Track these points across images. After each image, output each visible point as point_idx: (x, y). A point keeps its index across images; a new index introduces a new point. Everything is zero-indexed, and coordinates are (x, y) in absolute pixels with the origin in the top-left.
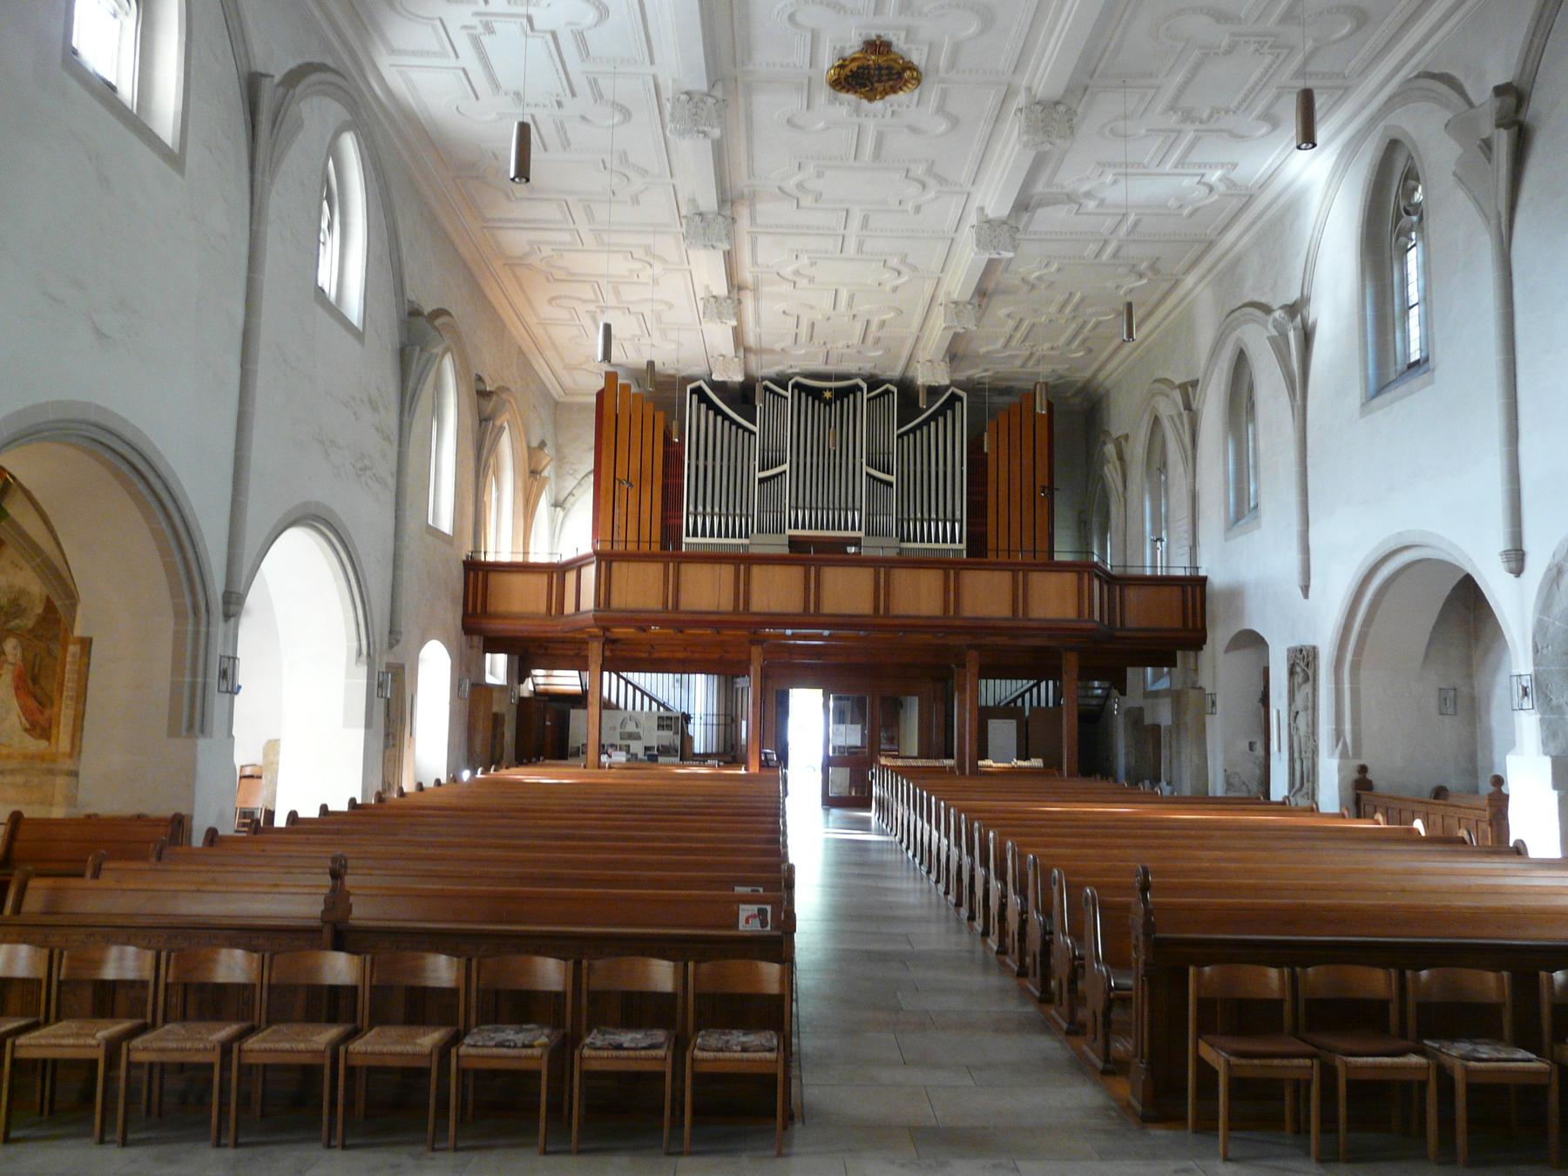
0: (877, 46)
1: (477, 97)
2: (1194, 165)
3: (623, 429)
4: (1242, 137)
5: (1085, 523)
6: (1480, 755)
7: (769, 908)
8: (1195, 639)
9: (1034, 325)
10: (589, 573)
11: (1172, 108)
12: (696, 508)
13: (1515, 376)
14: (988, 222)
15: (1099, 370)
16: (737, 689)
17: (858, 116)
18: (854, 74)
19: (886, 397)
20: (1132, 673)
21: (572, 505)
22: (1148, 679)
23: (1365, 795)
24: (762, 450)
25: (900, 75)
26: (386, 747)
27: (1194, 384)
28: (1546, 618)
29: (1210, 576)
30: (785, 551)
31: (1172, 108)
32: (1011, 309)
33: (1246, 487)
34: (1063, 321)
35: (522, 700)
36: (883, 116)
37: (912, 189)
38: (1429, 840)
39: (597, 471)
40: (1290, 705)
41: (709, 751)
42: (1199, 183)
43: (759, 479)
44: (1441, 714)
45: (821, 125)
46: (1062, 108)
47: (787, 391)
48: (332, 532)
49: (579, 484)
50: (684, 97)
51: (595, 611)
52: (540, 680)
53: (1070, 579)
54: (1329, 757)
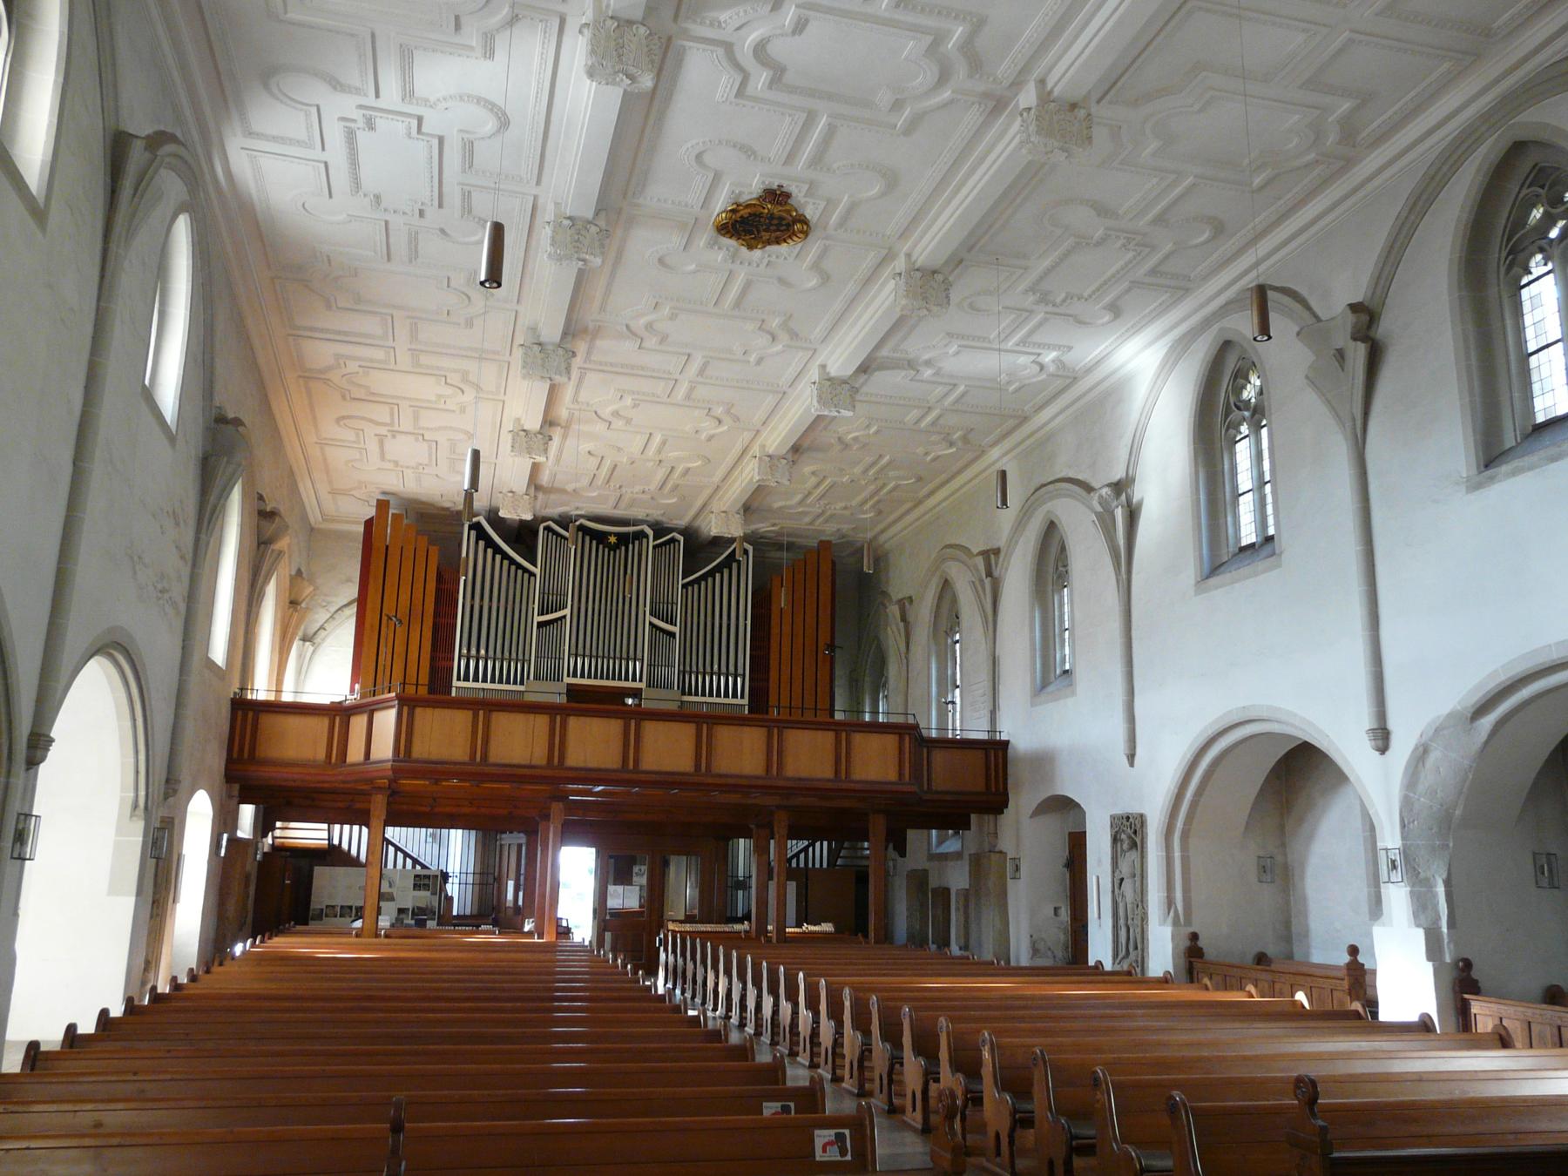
0: (777, 196)
1: (331, 196)
2: (1034, 344)
3: (407, 564)
4: (1085, 323)
5: (857, 681)
6: (1294, 921)
7: (847, 1132)
8: (994, 800)
9: (835, 483)
12: (469, 650)
13: (1373, 565)
14: (829, 380)
15: (882, 532)
16: (501, 845)
17: (733, 262)
18: (743, 220)
19: (672, 545)
20: (912, 835)
21: (323, 640)
22: (927, 843)
23: (1197, 965)
24: (542, 593)
25: (789, 226)
27: (997, 552)
28: (1412, 795)
29: (1012, 741)
30: (564, 699)
31: (1032, 289)
34: (863, 483)
36: (758, 266)
37: (762, 340)
39: (362, 601)
40: (1113, 872)
42: (1033, 362)
43: (538, 623)
44: (1261, 882)
45: (693, 267)
46: (939, 277)
48: (128, 662)
50: (567, 222)
51: (394, 761)
53: (891, 741)
54: (1160, 925)
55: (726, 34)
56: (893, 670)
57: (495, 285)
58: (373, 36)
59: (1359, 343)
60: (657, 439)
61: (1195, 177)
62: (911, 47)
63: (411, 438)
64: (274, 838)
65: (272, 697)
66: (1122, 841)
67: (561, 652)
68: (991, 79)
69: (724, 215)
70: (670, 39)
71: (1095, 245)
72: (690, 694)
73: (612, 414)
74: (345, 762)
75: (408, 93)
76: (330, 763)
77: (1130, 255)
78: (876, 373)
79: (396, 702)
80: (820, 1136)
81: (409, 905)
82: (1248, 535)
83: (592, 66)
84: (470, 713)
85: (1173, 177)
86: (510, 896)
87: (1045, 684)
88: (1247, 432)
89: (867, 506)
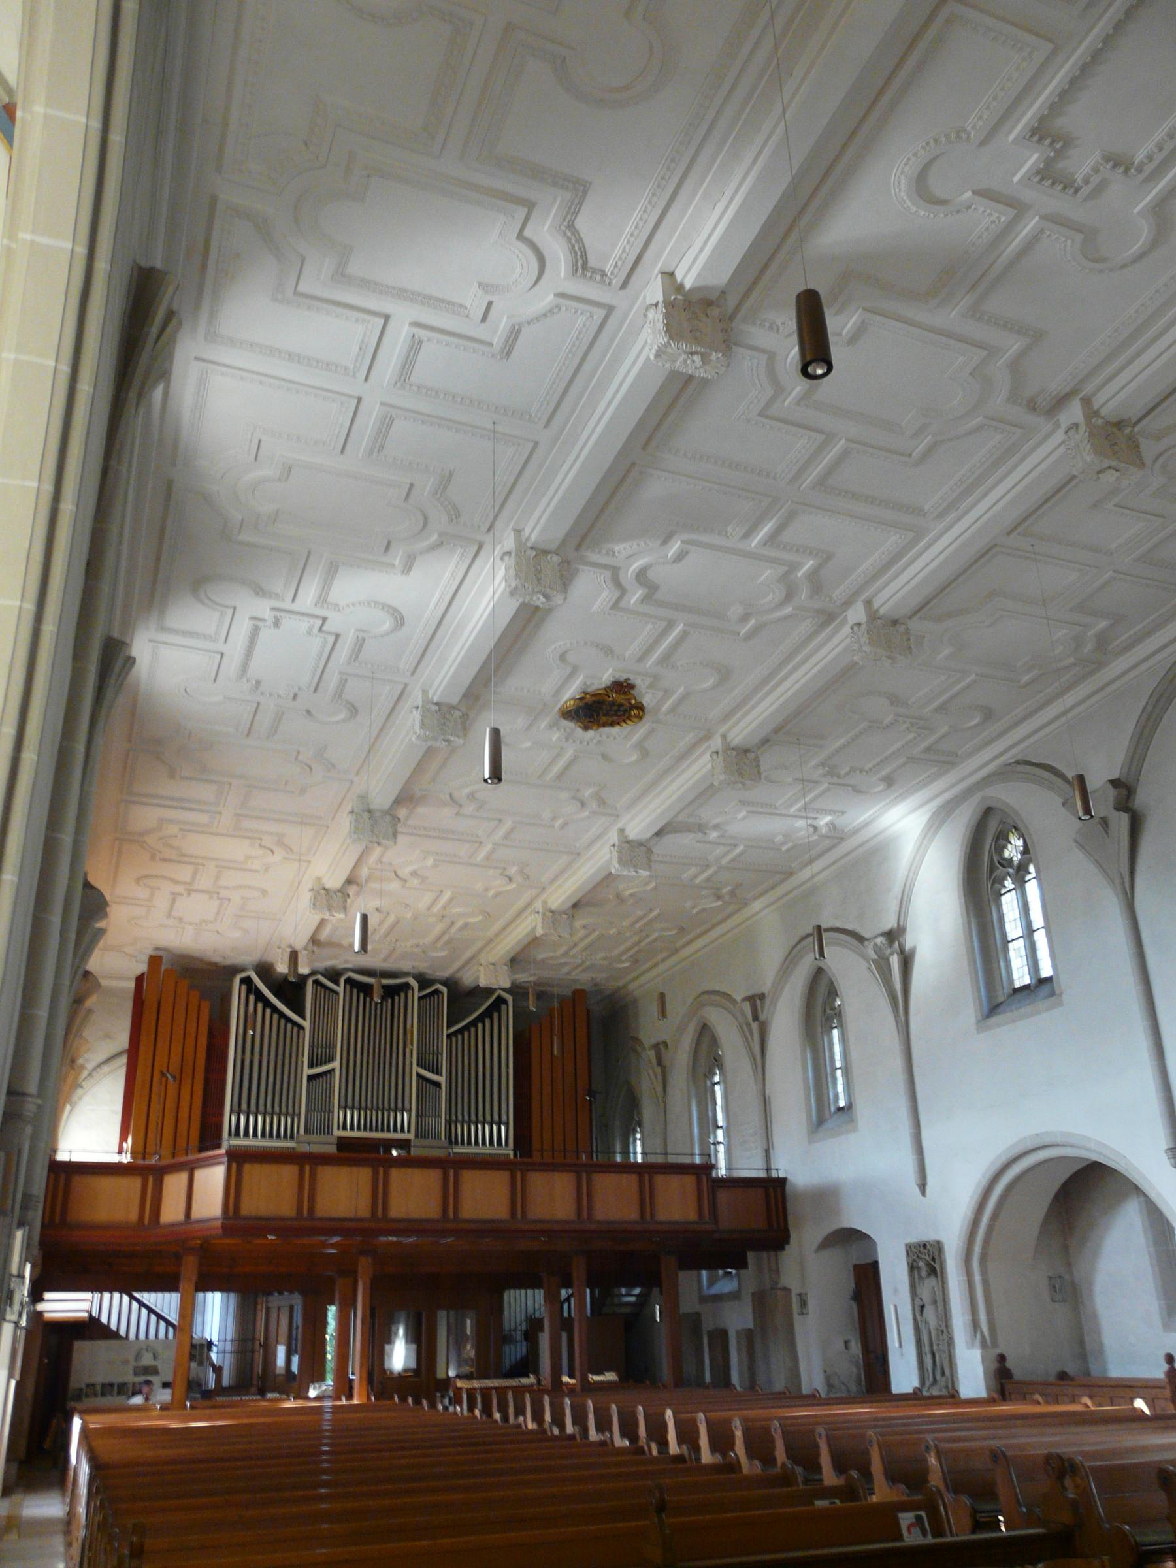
0: (623, 687)
1: (215, 680)
2: (814, 809)
3: (165, 1018)
7: (923, 1514)
11: (823, 764)
14: (628, 842)
21: (80, 1098)
23: (1009, 1387)
24: (312, 1047)
27: (762, 997)
29: (789, 1177)
33: (825, 1091)
38: (1155, 1418)
40: (913, 1300)
45: (528, 744)
53: (689, 1180)
54: (968, 1349)
57: (496, 781)
59: (1122, 813)
60: (447, 895)
61: (977, 675)
62: (768, 573)
63: (206, 896)
66: (919, 1268)
69: (572, 702)
73: (411, 874)
75: (322, 600)
77: (911, 736)
79: (226, 1159)
82: (1021, 977)
83: (516, 588)
86: (281, 1360)
87: (821, 1121)
88: (1012, 886)
89: (624, 958)
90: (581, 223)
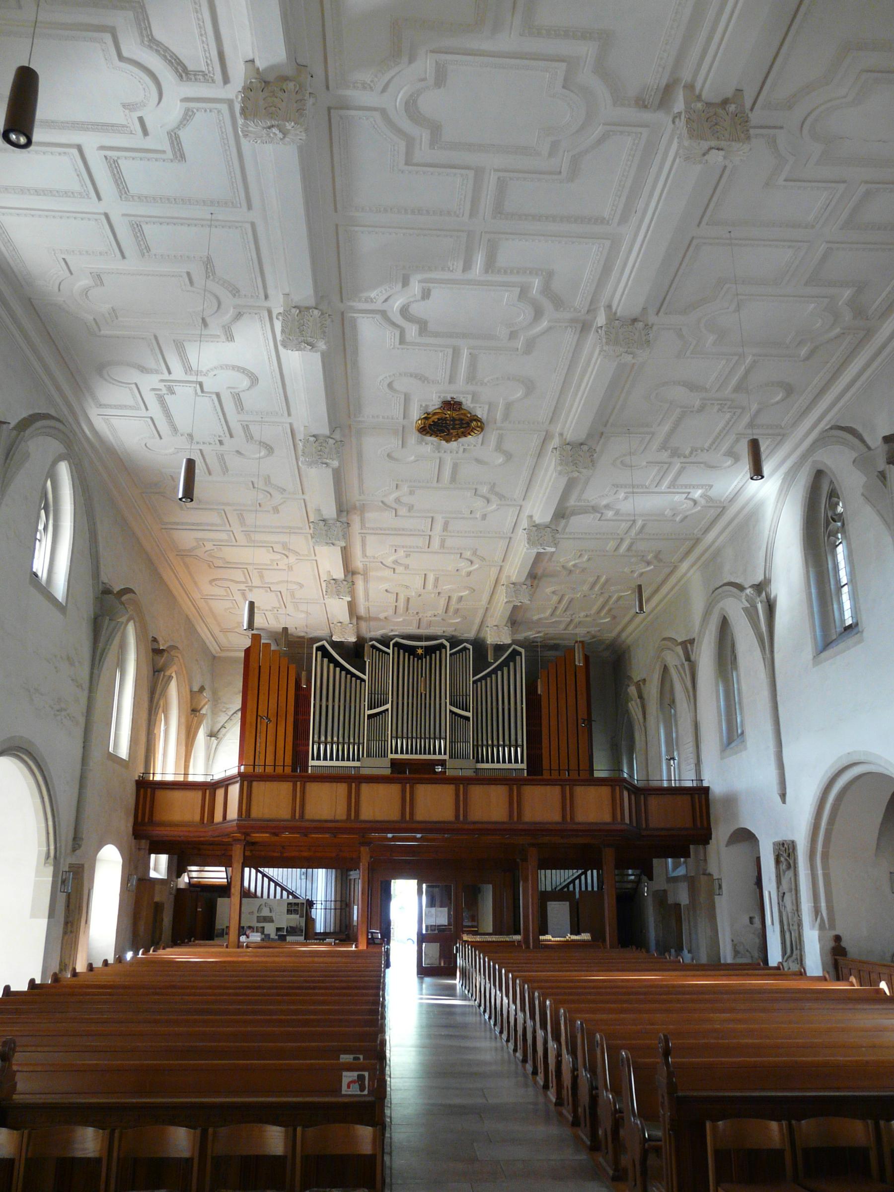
1: (161, 438)
2: (682, 486)
3: (274, 678)
7: (366, 1074)
8: (704, 836)
9: (572, 599)
10: (234, 790)
12: (319, 738)
15: (623, 630)
21: (224, 735)
24: (370, 694)
25: (468, 424)
26: (65, 933)
27: (692, 641)
29: (711, 787)
31: (663, 447)
32: (552, 589)
34: (594, 596)
35: (179, 890)
36: (457, 453)
37: (479, 503)
39: (244, 709)
40: (778, 888)
41: (328, 931)
42: (686, 498)
43: (368, 715)
45: (412, 458)
47: (389, 649)
49: (230, 719)
50: (312, 439)
52: (194, 875)
55: (378, 306)
56: (638, 737)
57: (189, 500)
58: (156, 338)
61: (754, 355)
64: (190, 878)
65: (181, 778)
67: (386, 735)
68: (572, 309)
69: (420, 422)
70: (342, 313)
71: (697, 412)
72: (483, 762)
74: (213, 822)
75: (188, 369)
76: (203, 823)
78: (572, 518)
79: (239, 778)
80: (346, 1076)
81: (284, 925)
82: (849, 622)
84: (291, 784)
85: (736, 358)
89: (602, 614)
90: (159, 33)
